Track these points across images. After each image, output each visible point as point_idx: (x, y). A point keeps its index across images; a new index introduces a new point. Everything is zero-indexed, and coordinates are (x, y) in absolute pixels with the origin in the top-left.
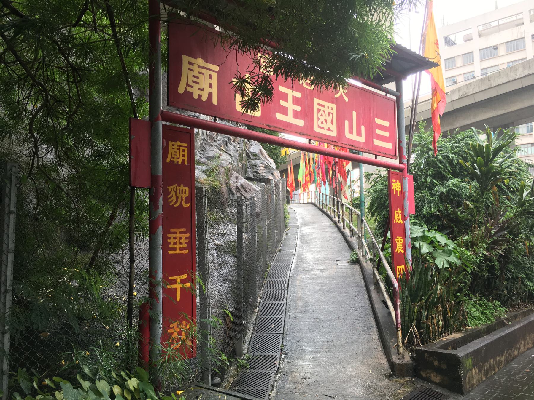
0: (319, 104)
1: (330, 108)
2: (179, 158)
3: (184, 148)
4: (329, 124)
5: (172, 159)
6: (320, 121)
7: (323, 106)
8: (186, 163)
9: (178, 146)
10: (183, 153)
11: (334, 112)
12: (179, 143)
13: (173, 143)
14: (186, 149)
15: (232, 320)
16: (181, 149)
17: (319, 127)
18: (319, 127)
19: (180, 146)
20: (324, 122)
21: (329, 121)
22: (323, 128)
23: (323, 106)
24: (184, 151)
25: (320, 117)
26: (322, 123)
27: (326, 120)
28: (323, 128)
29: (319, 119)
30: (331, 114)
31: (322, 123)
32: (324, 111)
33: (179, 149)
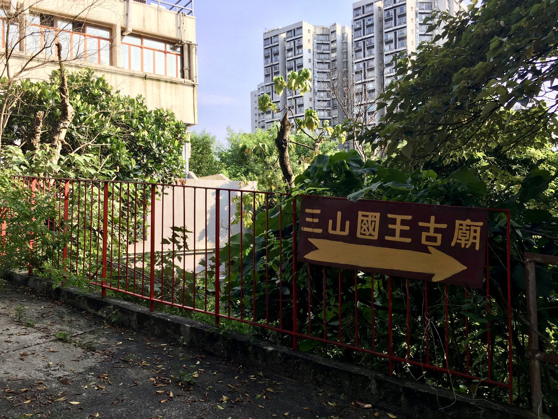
0: (363, 216)
1: (373, 217)
2: (468, 240)
3: (475, 228)
4: (371, 231)
5: (458, 241)
6: (363, 229)
7: (367, 216)
8: (477, 248)
9: (467, 226)
10: (475, 235)
11: (377, 220)
12: (468, 222)
13: (461, 222)
14: (479, 229)
15: (121, 343)
16: (473, 228)
17: (361, 234)
18: (361, 234)
19: (470, 226)
20: (366, 229)
21: (371, 228)
22: (365, 235)
23: (367, 216)
24: (475, 231)
25: (362, 225)
26: (364, 230)
27: (368, 228)
28: (365, 235)
29: (362, 227)
30: (373, 223)
31: (364, 230)
32: (367, 221)
33: (470, 230)
